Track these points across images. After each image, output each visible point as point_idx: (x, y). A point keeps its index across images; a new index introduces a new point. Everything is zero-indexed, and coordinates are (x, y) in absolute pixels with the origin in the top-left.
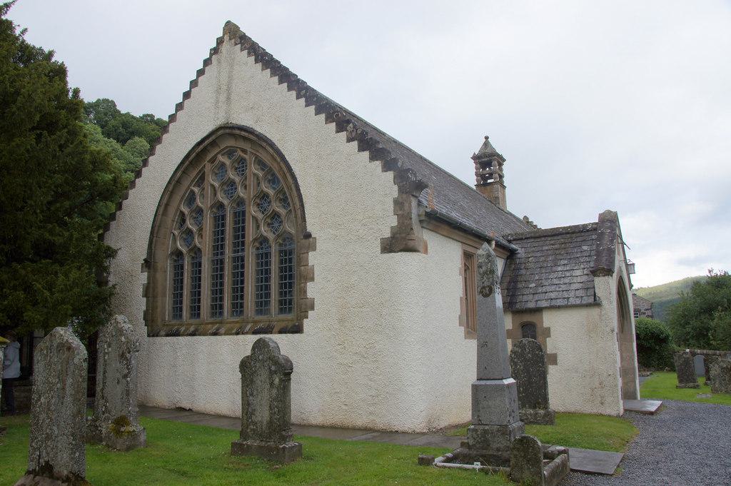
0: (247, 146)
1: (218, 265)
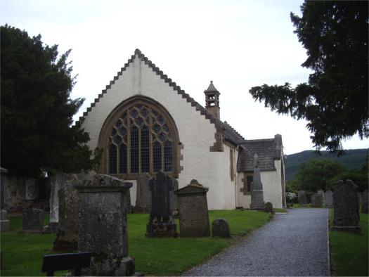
0: (147, 104)
1: (134, 153)
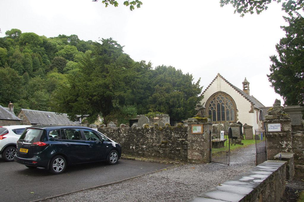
1: (219, 113)
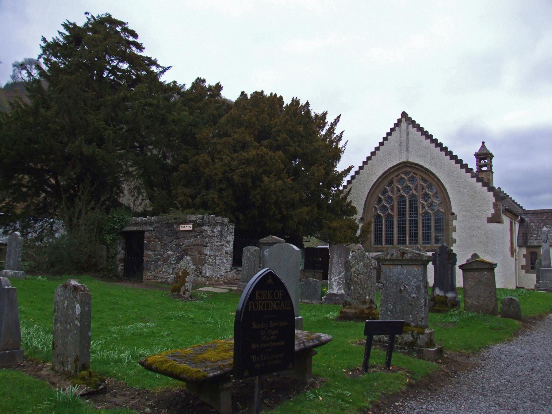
0: (415, 171)
1: (402, 224)
